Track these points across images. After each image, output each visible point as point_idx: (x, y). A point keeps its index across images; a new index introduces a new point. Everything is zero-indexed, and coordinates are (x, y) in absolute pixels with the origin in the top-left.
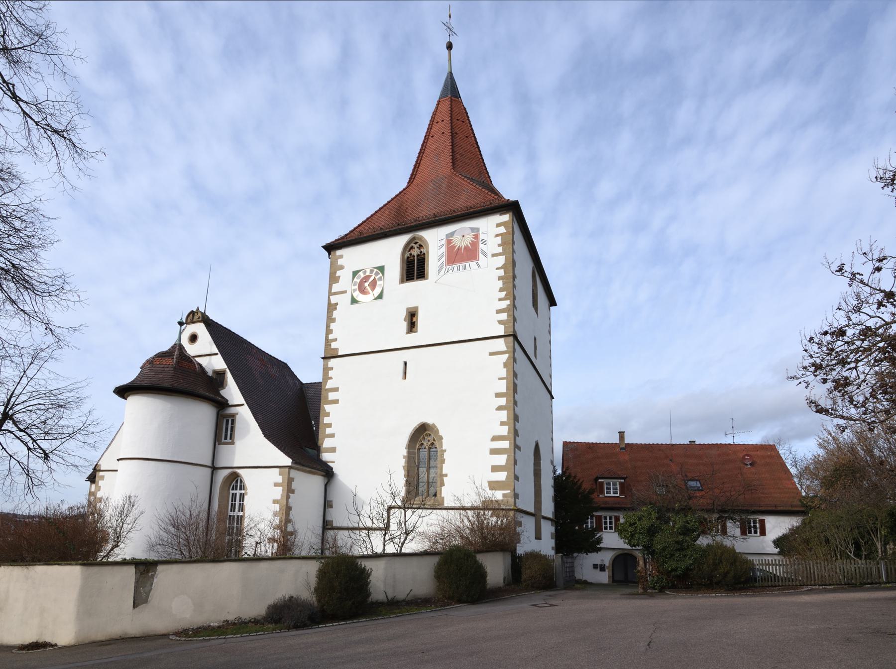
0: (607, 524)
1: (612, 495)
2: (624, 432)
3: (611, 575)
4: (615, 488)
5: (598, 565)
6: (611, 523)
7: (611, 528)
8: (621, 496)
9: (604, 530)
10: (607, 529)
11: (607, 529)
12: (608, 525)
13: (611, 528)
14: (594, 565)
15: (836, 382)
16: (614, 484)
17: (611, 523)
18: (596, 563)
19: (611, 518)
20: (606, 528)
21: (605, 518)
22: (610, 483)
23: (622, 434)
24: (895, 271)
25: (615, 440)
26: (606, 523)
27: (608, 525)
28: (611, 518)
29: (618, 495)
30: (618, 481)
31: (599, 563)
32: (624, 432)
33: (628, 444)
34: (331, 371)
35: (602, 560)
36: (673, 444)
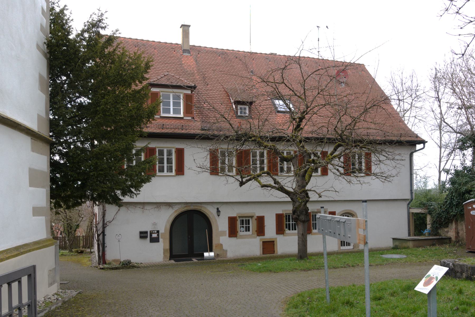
0: (168, 158)
1: (172, 115)
2: (189, 26)
3: (168, 247)
4: (177, 104)
5: (146, 232)
6: (169, 161)
7: (170, 169)
8: (185, 118)
9: (158, 174)
10: (163, 171)
11: (163, 171)
12: (165, 165)
13: (170, 169)
14: (141, 233)
15: (71, 251)
16: (177, 97)
17: (169, 161)
18: (143, 230)
19: (169, 153)
20: (162, 170)
21: (161, 153)
22: (169, 95)
23: (186, 28)
24: (25, 311)
25: (177, 39)
26: (161, 161)
27: (165, 165)
28: (169, 153)
29: (182, 115)
30: (182, 93)
31: (148, 228)
32: (189, 26)
33: (194, 47)
34: (223, 237)
35: (155, 224)
36: (252, 53)
